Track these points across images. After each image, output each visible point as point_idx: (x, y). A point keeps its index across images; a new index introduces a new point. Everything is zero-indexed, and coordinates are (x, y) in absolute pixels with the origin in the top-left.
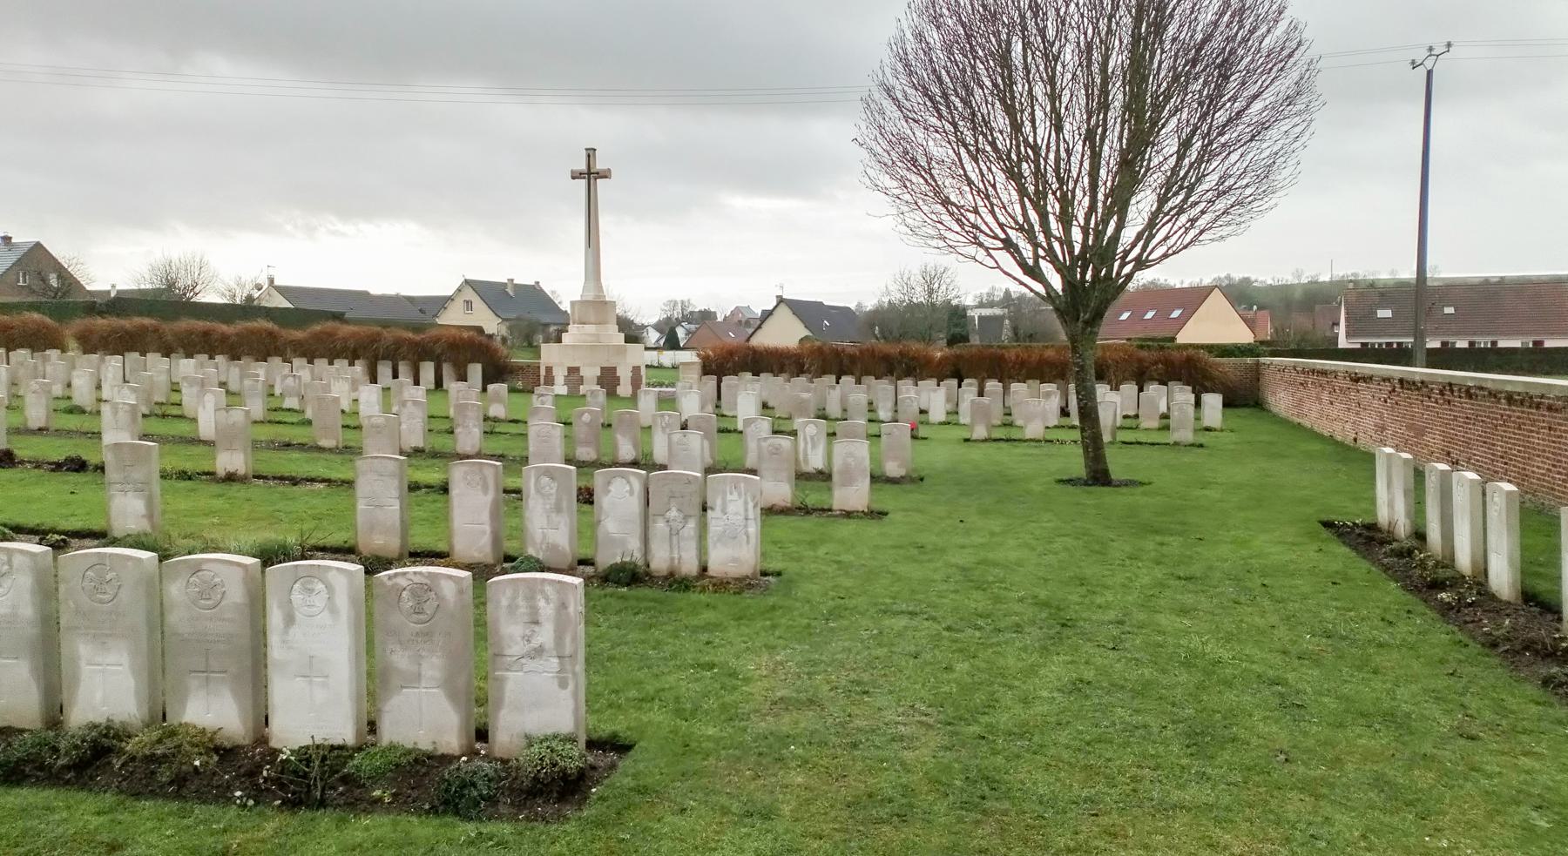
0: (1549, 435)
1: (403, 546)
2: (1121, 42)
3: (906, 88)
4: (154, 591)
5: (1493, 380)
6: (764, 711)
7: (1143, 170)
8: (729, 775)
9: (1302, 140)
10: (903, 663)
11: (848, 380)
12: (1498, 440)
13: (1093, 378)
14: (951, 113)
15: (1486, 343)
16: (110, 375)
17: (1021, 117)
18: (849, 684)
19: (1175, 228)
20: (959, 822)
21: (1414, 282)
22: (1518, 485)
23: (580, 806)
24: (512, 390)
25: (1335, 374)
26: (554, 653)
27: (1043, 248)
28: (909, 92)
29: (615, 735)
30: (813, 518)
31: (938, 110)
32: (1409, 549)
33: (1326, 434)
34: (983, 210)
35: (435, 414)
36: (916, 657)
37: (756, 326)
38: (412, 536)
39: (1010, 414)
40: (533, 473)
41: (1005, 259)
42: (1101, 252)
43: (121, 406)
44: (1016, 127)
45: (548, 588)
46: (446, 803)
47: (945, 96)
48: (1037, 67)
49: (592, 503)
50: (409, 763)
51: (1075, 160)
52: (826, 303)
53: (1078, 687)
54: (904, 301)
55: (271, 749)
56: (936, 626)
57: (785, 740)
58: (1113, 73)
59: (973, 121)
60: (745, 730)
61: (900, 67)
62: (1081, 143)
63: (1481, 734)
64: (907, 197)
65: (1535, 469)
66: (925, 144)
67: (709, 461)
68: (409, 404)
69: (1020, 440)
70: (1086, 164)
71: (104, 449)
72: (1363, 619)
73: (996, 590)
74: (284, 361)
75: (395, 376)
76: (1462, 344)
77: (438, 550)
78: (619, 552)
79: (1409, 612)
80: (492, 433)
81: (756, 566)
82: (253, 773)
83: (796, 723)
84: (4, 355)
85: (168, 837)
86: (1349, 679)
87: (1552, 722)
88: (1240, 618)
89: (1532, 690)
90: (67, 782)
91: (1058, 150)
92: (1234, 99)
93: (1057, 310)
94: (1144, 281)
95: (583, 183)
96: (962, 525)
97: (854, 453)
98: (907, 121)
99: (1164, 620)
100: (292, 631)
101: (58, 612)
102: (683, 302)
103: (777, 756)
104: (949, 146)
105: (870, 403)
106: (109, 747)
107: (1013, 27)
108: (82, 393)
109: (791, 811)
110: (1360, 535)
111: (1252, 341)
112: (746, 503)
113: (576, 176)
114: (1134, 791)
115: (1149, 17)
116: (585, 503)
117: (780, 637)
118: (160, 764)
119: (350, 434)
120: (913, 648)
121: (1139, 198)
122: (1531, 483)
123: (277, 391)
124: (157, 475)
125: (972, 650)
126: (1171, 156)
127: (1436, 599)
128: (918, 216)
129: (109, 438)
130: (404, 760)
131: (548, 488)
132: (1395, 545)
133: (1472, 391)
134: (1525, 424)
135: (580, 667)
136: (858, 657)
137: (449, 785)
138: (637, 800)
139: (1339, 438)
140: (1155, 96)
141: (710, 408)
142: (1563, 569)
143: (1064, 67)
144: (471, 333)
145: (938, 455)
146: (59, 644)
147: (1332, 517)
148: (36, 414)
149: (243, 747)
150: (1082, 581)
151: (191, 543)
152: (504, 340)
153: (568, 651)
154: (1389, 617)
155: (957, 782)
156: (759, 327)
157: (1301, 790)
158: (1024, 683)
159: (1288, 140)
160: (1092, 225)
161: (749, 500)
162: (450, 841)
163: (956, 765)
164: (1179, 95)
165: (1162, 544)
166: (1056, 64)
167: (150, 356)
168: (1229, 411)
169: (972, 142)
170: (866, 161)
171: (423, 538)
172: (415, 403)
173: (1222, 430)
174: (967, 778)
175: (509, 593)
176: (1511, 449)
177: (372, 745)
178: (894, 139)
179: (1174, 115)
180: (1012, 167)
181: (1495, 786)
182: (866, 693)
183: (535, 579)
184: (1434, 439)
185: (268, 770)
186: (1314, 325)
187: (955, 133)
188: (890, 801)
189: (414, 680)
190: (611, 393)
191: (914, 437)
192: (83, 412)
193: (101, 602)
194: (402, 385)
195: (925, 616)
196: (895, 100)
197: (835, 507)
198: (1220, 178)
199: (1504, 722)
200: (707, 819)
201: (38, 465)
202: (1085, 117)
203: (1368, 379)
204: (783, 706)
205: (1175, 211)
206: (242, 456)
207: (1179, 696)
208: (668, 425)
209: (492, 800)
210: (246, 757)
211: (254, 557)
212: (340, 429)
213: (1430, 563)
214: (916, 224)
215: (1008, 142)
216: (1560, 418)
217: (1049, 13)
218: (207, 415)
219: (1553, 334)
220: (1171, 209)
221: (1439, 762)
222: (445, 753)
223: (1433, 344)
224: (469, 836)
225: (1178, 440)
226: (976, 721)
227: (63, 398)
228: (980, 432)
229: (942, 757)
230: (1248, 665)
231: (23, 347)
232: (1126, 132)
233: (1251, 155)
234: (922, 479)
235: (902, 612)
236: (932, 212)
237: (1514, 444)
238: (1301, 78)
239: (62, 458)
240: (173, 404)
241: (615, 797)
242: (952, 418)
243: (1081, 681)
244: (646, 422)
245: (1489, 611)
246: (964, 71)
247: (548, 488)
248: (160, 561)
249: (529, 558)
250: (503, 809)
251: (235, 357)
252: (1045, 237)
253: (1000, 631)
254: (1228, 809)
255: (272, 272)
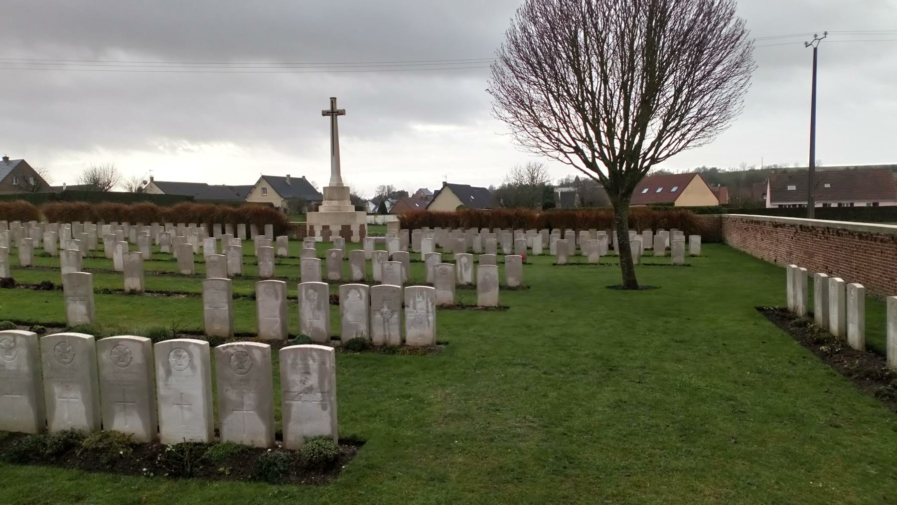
0: (881, 256)
1: (230, 330)
2: (641, 31)
3: (517, 59)
4: (93, 354)
5: (851, 225)
6: (439, 421)
7: (655, 106)
8: (420, 457)
9: (746, 87)
10: (519, 393)
11: (485, 231)
12: (854, 260)
13: (627, 228)
14: (543, 74)
15: (847, 204)
16: (64, 235)
17: (584, 76)
18: (488, 406)
19: (673, 139)
20: (551, 481)
21: (808, 169)
22: (864, 284)
23: (336, 476)
24: (290, 240)
25: (764, 222)
26: (319, 390)
27: (598, 152)
28: (518, 61)
29: (354, 436)
30: (467, 311)
31: (536, 72)
32: (805, 322)
33: (759, 257)
34: (563, 131)
35: (247, 254)
36: (526, 390)
37: (431, 200)
38: (236, 324)
39: (579, 249)
40: (304, 287)
41: (576, 158)
42: (631, 153)
43: (71, 252)
44: (581, 81)
45: (314, 353)
46: (260, 474)
47: (539, 63)
48: (593, 46)
49: (338, 304)
50: (239, 452)
51: (615, 100)
52: (472, 186)
53: (619, 405)
54: (517, 184)
55: (162, 445)
56: (538, 371)
57: (452, 437)
58: (636, 49)
59: (556, 78)
60: (429, 432)
61: (513, 47)
62: (618, 90)
63: (842, 424)
64: (518, 123)
65: (873, 275)
66: (528, 91)
67: (405, 278)
68: (232, 248)
69: (585, 264)
70: (622, 103)
71: (62, 277)
72: (779, 362)
73: (572, 351)
74: (161, 225)
75: (224, 232)
76: (834, 205)
77: (251, 332)
78: (354, 332)
79: (804, 357)
80: (279, 264)
81: (433, 339)
82: (153, 458)
83: (458, 428)
84: (7, 225)
85: (108, 493)
86: (770, 396)
87: (879, 416)
88: (710, 363)
89: (869, 399)
90: (52, 463)
91: (605, 95)
92: (706, 64)
93: (606, 188)
94: (656, 171)
95: (329, 118)
96: (552, 313)
97: (489, 272)
98: (517, 79)
99: (667, 365)
100: (170, 379)
101: (42, 369)
102: (388, 187)
103: (447, 446)
104: (542, 93)
105: (498, 244)
106: (73, 444)
107: (578, 23)
108: (49, 244)
109: (456, 477)
110: (778, 315)
111: (717, 204)
112: (427, 303)
113: (325, 114)
114: (651, 462)
115: (657, 16)
116: (334, 304)
117: (448, 380)
118: (101, 453)
119: (199, 266)
120: (524, 385)
121: (652, 122)
122: (872, 283)
123: (157, 242)
124: (92, 291)
125: (559, 384)
126: (671, 97)
127: (819, 350)
128: (525, 134)
129: (65, 271)
130: (236, 451)
131: (312, 296)
132: (797, 320)
133: (840, 232)
134: (868, 250)
135: (333, 398)
136: (493, 390)
137: (262, 464)
138: (368, 472)
139: (766, 260)
140: (661, 63)
141: (405, 248)
142: (888, 331)
143: (608, 46)
144: (266, 207)
145: (538, 274)
146: (43, 387)
147: (762, 305)
148: (25, 258)
149: (146, 444)
150: (621, 345)
151: (113, 329)
152: (285, 210)
153: (327, 388)
154: (793, 361)
155: (550, 459)
156: (433, 200)
157: (744, 459)
158: (589, 403)
159: (737, 88)
160: (626, 138)
161: (429, 301)
162: (263, 496)
163: (550, 450)
164: (674, 62)
165: (667, 322)
166: (603, 45)
167: (85, 223)
168: (705, 245)
169: (556, 90)
170: (494, 102)
171: (242, 326)
172: (235, 248)
173: (701, 256)
174: (556, 457)
175: (292, 356)
176: (860, 264)
177: (218, 443)
178: (510, 89)
179: (672, 73)
180: (579, 105)
181: (848, 452)
182: (498, 410)
183: (307, 348)
184: (819, 259)
185: (160, 456)
186: (752, 195)
187: (546, 85)
188: (512, 470)
189: (240, 406)
190: (348, 240)
191: (524, 263)
192: (50, 256)
193: (65, 363)
194: (227, 238)
195: (532, 366)
196: (510, 66)
197: (478, 304)
198: (699, 110)
199: (854, 417)
200: (408, 483)
201: (27, 286)
202: (621, 75)
203: (782, 225)
204: (450, 418)
205: (673, 129)
206: (138, 280)
207: (676, 408)
208: (381, 258)
209: (286, 473)
210: (148, 449)
211: (148, 337)
212: (193, 264)
213: (816, 330)
214: (524, 139)
215: (576, 90)
216: (887, 246)
217: (599, 15)
218: (118, 257)
219: (885, 198)
220: (671, 128)
221: (819, 440)
222: (259, 447)
223: (819, 205)
224: (274, 493)
225: (676, 262)
226: (561, 425)
227: (39, 248)
228: (562, 259)
229: (542, 446)
230: (715, 390)
231: (16, 220)
232: (645, 83)
233: (716, 97)
234: (529, 288)
235: (518, 364)
236: (533, 132)
237: (863, 262)
238: (744, 52)
239: (40, 283)
240: (99, 251)
241: (355, 470)
242: (546, 252)
243: (621, 401)
244: (368, 256)
245: (848, 356)
246: (550, 49)
247: (312, 296)
248: (96, 340)
249: (303, 336)
250: (293, 478)
251: (133, 223)
252: (599, 145)
253: (574, 374)
254: (702, 470)
255: (152, 174)
